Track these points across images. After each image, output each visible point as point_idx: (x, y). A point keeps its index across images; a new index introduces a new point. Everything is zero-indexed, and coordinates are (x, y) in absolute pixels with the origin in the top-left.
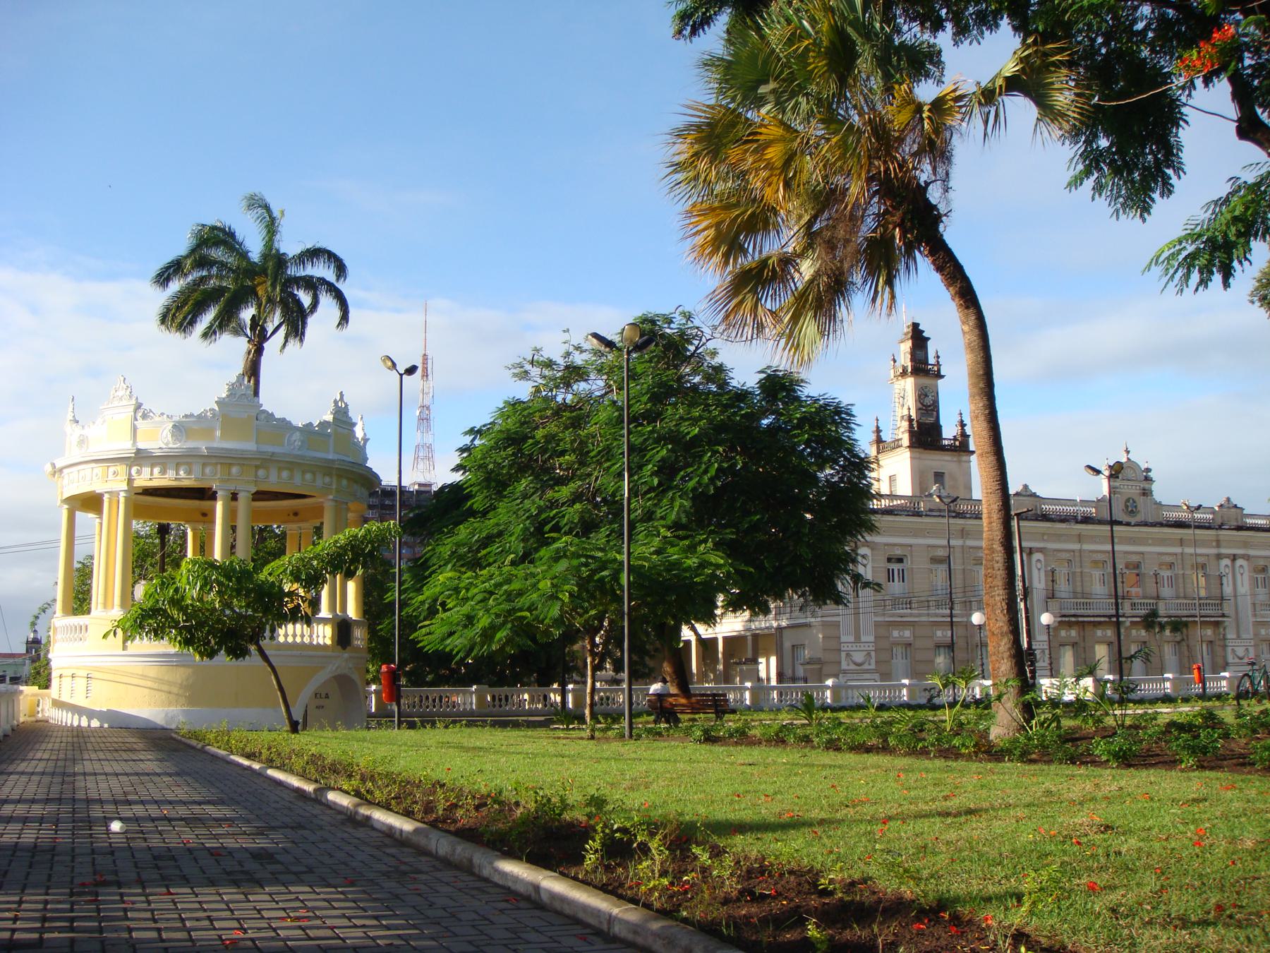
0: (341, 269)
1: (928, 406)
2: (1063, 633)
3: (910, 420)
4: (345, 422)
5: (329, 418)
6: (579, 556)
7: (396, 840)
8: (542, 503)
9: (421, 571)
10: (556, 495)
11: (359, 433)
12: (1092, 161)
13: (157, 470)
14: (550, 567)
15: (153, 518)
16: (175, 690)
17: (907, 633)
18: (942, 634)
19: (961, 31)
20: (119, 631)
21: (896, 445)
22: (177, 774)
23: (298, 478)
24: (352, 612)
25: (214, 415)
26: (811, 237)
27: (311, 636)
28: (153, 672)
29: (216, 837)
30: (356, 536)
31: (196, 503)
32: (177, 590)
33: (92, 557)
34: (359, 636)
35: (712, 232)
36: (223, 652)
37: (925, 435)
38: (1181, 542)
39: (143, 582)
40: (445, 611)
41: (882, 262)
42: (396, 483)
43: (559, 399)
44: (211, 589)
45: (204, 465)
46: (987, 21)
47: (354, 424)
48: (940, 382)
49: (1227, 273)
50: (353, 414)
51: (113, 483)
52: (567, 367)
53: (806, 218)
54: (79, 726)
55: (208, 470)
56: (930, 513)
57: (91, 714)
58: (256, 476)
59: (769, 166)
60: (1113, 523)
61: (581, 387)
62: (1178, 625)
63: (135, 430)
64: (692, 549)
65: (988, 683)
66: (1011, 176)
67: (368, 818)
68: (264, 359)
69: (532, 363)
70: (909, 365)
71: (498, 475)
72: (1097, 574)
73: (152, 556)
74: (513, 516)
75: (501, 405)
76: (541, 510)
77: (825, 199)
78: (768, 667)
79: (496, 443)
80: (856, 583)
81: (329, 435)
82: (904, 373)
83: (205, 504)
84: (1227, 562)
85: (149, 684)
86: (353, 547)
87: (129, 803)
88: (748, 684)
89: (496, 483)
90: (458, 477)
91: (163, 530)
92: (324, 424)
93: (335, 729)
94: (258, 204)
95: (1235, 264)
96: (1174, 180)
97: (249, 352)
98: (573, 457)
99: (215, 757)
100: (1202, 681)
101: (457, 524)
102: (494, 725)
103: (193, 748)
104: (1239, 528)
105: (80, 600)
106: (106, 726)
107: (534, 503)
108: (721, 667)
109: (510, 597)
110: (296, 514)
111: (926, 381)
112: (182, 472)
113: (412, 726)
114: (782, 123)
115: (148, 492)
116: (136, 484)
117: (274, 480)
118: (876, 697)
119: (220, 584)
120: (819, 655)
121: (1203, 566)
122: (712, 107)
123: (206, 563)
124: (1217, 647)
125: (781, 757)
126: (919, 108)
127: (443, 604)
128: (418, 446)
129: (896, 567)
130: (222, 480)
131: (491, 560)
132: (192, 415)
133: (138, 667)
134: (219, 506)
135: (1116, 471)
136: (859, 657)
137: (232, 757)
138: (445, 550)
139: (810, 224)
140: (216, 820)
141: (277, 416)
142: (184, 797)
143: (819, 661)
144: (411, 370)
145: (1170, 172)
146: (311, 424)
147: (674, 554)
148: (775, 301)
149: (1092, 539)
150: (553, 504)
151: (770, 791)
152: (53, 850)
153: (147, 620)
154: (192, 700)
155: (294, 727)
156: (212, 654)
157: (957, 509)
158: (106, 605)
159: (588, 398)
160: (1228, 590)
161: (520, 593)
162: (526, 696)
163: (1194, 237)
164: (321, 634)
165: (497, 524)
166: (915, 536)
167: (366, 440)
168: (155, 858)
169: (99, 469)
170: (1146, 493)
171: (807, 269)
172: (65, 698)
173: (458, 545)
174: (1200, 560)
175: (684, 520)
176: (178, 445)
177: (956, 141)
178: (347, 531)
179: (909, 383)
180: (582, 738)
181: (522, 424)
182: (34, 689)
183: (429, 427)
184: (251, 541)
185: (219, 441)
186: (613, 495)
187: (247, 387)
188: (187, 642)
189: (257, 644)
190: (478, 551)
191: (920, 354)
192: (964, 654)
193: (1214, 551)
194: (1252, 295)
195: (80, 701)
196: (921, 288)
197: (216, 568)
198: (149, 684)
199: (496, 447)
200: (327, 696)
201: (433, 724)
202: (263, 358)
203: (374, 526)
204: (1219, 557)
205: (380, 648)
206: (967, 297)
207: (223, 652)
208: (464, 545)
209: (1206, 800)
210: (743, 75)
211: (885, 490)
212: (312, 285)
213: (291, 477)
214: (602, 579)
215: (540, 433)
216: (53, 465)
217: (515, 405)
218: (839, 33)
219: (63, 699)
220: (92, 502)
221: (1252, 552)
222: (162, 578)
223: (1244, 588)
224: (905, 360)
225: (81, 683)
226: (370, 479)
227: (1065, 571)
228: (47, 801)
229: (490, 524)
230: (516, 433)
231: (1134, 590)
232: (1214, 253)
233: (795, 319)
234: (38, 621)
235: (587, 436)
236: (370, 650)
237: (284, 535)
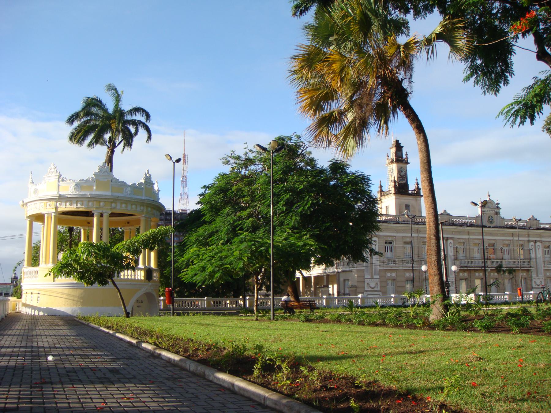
0: (148, 117)
1: (403, 176)
2: (461, 274)
3: (395, 182)
4: (150, 183)
5: (143, 181)
6: (251, 241)
7: (172, 364)
8: (235, 218)
9: (183, 247)
10: (241, 214)
11: (156, 188)
12: (474, 70)
13: (68, 204)
14: (239, 246)
15: (66, 224)
16: (76, 299)
17: (394, 274)
18: (409, 275)
19: (417, 14)
20: (52, 274)
21: (389, 193)
22: (77, 335)
23: (129, 207)
24: (153, 265)
25: (93, 180)
26: (352, 103)
27: (135, 276)
28: (66, 291)
29: (94, 363)
30: (155, 232)
31: (85, 218)
32: (77, 256)
33: (40, 242)
34: (156, 276)
35: (309, 101)
36: (97, 282)
37: (401, 188)
38: (513, 235)
39: (62, 252)
40: (193, 265)
41: (383, 113)
42: (172, 209)
43: (243, 173)
44: (92, 255)
45: (89, 202)
46: (428, 9)
47: (154, 184)
48: (408, 165)
49: (532, 118)
50: (153, 180)
51: (49, 209)
52: (246, 159)
53: (350, 94)
54: (34, 314)
55: (90, 204)
56: (404, 222)
57: (39, 309)
58: (111, 206)
59: (334, 72)
60: (483, 226)
61: (252, 168)
62: (511, 271)
63: (58, 186)
64: (300, 238)
65: (429, 296)
66: (439, 76)
67: (160, 355)
68: (114, 156)
69: (231, 157)
70: (394, 158)
71: (216, 206)
72: (476, 249)
73: (66, 241)
74: (223, 224)
75: (218, 176)
76: (235, 221)
77: (358, 86)
78: (333, 289)
79: (215, 192)
80: (371, 253)
81: (143, 189)
82: (392, 162)
83: (89, 218)
84: (532, 243)
85: (65, 296)
86: (153, 237)
87: (56, 348)
88: (325, 297)
89: (215, 209)
90: (199, 207)
91: (71, 230)
92: (140, 184)
93: (145, 316)
94: (112, 88)
95: (536, 114)
96: (509, 78)
97: (108, 153)
98: (249, 198)
99: (93, 328)
100: (522, 295)
101: (198, 227)
102: (214, 314)
103: (84, 324)
104: (538, 229)
105: (35, 260)
106: (46, 314)
107: (232, 218)
108: (313, 289)
109: (221, 259)
110: (128, 223)
111: (402, 165)
112: (79, 205)
113: (179, 315)
114: (339, 53)
115: (64, 213)
116: (59, 210)
117: (119, 208)
118: (380, 302)
119: (95, 253)
120: (355, 284)
121: (522, 245)
122: (309, 46)
123: (89, 244)
124: (528, 280)
125: (339, 328)
126: (399, 47)
127: (192, 262)
128: (181, 193)
129: (389, 246)
130: (96, 208)
131: (213, 243)
132: (83, 180)
133: (60, 289)
134: (95, 219)
135: (484, 204)
136: (373, 285)
137: (101, 328)
138: (193, 238)
139: (351, 97)
140: (94, 355)
141: (120, 180)
142: (80, 346)
143: (355, 287)
144: (178, 161)
145: (507, 74)
146: (135, 184)
147: (292, 240)
148: (336, 130)
149: (474, 234)
150: (240, 218)
151: (334, 343)
153: (64, 269)
154: (83, 304)
155: (128, 315)
156: (92, 284)
157: (415, 220)
158: (46, 262)
159: (255, 173)
160: (533, 256)
161: (226, 257)
162: (228, 302)
163: (518, 103)
164: (139, 275)
165: (216, 227)
166: (397, 232)
167: (159, 191)
168: (67, 372)
169: (43, 203)
170: (497, 214)
171: (350, 116)
172: (28, 302)
173: (199, 236)
174: (521, 243)
175: (297, 225)
176: (77, 193)
177: (415, 61)
178: (151, 230)
179: (394, 166)
180: (252, 320)
181: (227, 184)
182: (15, 299)
183: (186, 185)
184: (109, 234)
185: (95, 191)
186: (266, 214)
187: (107, 168)
188: (81, 278)
189: (112, 279)
190: (207, 239)
191: (399, 153)
192: (418, 283)
193: (526, 239)
194: (543, 128)
195: (35, 304)
196: (400, 125)
197: (94, 246)
198: (65, 296)
199: (215, 194)
200: (142, 302)
201: (188, 314)
202: (114, 155)
203: (162, 228)
204: (529, 241)
205: (165, 281)
206: (420, 129)
207: (97, 282)
208: (201, 236)
209: (523, 347)
210: (323, 32)
211: (384, 212)
212: (135, 123)
213: (126, 207)
214: (261, 251)
215: (234, 188)
216: (23, 202)
217: (223, 175)
218: (364, 14)
219: (27, 303)
220: (40, 218)
221: (543, 239)
222: (70, 250)
223: (540, 255)
224: (393, 156)
225: (35, 296)
226: (160, 208)
227: (462, 247)
228: (20, 347)
229: (213, 227)
230: (224, 188)
231: (492, 256)
232: (527, 110)
233: (345, 138)
234: (17, 269)
235: (255, 189)
236: (161, 282)
237: (123, 232)
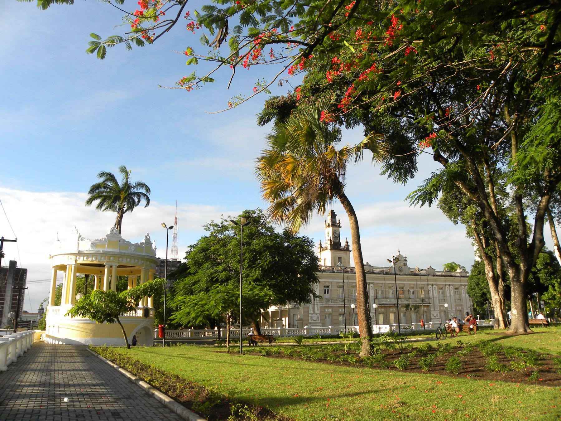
0: (148, 190)
1: (336, 236)
2: (380, 310)
3: (331, 241)
5: (144, 241)
6: (224, 292)
7: (162, 404)
9: (173, 292)
11: (153, 246)
12: (389, 166)
13: (85, 258)
16: (89, 332)
17: (330, 310)
18: (342, 311)
19: (349, 125)
20: (70, 314)
21: (326, 248)
22: (88, 370)
23: (133, 261)
24: (150, 305)
26: (301, 191)
28: (81, 325)
29: (100, 403)
31: (98, 268)
32: (90, 300)
34: (152, 313)
35: (269, 190)
37: (335, 245)
38: (416, 280)
41: (322, 199)
43: (219, 236)
45: (101, 256)
46: (356, 122)
48: (340, 229)
49: (430, 203)
50: (152, 240)
51: (70, 261)
53: (300, 185)
55: (102, 258)
56: (338, 271)
57: (59, 340)
59: (288, 171)
60: (395, 274)
61: (227, 233)
62: (417, 307)
63: (78, 244)
64: (262, 290)
65: (357, 327)
66: (365, 175)
67: (153, 394)
70: (330, 223)
72: (390, 290)
73: (84, 286)
74: (203, 275)
76: (212, 274)
77: (305, 181)
78: (285, 321)
80: (314, 296)
82: (329, 226)
83: (101, 268)
84: (430, 286)
87: (69, 386)
88: (279, 328)
89: (198, 264)
90: (185, 261)
91: (87, 276)
92: (142, 243)
94: (124, 170)
95: (433, 199)
96: (415, 173)
98: (223, 257)
99: (101, 360)
100: (424, 325)
103: (94, 355)
104: (434, 276)
105: (57, 301)
108: (270, 321)
109: (203, 306)
111: (336, 228)
113: (169, 345)
114: (293, 157)
116: (78, 262)
117: (124, 262)
118: (320, 332)
120: (302, 317)
121: (423, 288)
122: (271, 151)
124: (428, 313)
125: (293, 364)
126: (336, 153)
127: (180, 308)
129: (326, 289)
130: (107, 262)
133: (76, 324)
135: (396, 260)
136: (315, 318)
138: (181, 286)
139: (301, 187)
140: (100, 394)
142: (89, 382)
143: (302, 320)
145: (413, 170)
147: (256, 291)
148: (289, 213)
149: (389, 279)
150: (216, 272)
151: (289, 384)
152: (39, 413)
153: (80, 310)
154: (94, 335)
155: (129, 347)
156: (102, 322)
157: (347, 271)
158: (66, 302)
159: (228, 237)
160: (431, 295)
161: (206, 304)
163: (420, 190)
166: (333, 279)
167: (156, 249)
168: (77, 416)
170: (405, 265)
171: (299, 201)
172: (51, 334)
173: (185, 284)
174: (422, 286)
175: (259, 278)
177: (347, 164)
179: (330, 229)
180: (225, 352)
182: (40, 331)
185: (107, 249)
186: (236, 268)
190: (192, 286)
191: (334, 220)
192: (349, 317)
193: (426, 283)
194: (438, 205)
196: (336, 205)
203: (158, 280)
204: (428, 285)
206: (351, 212)
209: (433, 389)
210: (280, 141)
211: (323, 264)
212: (139, 195)
213: (130, 261)
214: (232, 300)
215: (213, 248)
217: (205, 238)
218: (310, 128)
220: (63, 268)
221: (438, 283)
223: (436, 294)
224: (329, 221)
227: (380, 290)
228: (40, 385)
229: (195, 278)
231: (401, 296)
232: (426, 196)
233: (295, 217)
235: (228, 250)
236: (155, 316)
237: (128, 277)
